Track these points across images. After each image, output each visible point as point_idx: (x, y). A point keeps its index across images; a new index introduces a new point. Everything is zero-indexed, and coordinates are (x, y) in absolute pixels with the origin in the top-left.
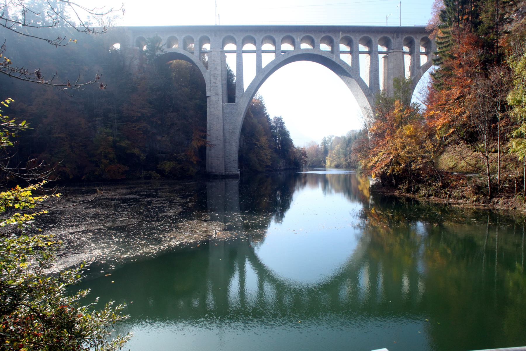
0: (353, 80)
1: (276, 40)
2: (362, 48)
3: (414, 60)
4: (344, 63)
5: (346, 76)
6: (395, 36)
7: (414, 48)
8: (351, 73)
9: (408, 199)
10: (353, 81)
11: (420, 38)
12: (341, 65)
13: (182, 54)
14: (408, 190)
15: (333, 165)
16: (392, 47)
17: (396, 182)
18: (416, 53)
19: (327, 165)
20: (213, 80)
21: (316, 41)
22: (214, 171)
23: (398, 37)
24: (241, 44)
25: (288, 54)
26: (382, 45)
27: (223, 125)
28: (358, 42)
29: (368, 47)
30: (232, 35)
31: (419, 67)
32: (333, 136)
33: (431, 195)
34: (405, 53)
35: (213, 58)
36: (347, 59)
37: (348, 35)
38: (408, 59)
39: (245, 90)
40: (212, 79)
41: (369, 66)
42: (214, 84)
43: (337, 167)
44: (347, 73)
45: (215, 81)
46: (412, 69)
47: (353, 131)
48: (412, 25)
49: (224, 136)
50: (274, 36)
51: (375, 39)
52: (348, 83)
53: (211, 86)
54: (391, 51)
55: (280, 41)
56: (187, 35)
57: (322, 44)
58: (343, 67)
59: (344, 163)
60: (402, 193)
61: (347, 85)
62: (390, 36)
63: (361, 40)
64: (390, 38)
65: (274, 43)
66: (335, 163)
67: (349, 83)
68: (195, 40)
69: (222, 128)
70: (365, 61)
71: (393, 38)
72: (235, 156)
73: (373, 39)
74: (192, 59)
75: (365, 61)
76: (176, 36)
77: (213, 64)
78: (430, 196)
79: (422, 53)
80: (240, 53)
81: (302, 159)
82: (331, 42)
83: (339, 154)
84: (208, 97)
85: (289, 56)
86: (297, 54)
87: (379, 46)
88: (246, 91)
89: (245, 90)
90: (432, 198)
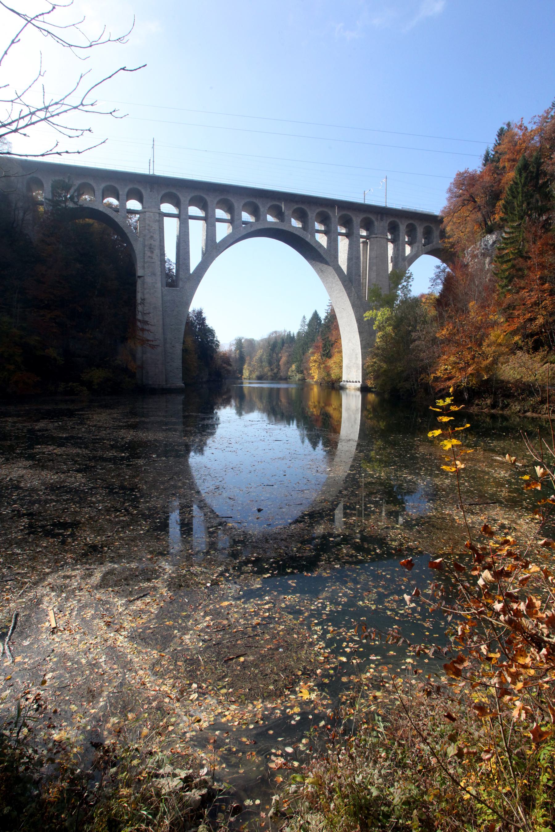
0: (331, 268)
1: (182, 199)
2: (220, 213)
3: (398, 250)
4: (321, 246)
5: (321, 262)
6: (379, 218)
7: (399, 235)
8: (328, 259)
9: (493, 417)
10: (330, 270)
11: (406, 224)
12: (316, 247)
13: (100, 211)
14: (494, 406)
15: (254, 376)
16: (376, 232)
17: (470, 397)
18: (400, 242)
19: (244, 376)
20: (148, 254)
21: (262, 209)
22: (150, 383)
23: (382, 220)
24: (101, 198)
25: (251, 226)
26: (296, 219)
27: (163, 319)
28: (215, 205)
29: (302, 222)
30: (174, 191)
31: (404, 258)
32: (243, 338)
33: (528, 411)
34: (388, 240)
35: (147, 222)
36: (322, 240)
37: (349, 213)
38: (390, 246)
39: (191, 272)
40: (146, 252)
41: (347, 252)
42: (149, 260)
43: (260, 378)
44: (324, 259)
45: (150, 255)
46: (395, 259)
47: (276, 332)
48: (399, 207)
49: (164, 333)
50: (209, 199)
51: (237, 204)
52: (320, 272)
53: (144, 262)
54: (374, 236)
55: (160, 198)
56: (108, 184)
57: (291, 218)
58: (319, 250)
59: (269, 374)
60: (482, 409)
61: (318, 274)
62: (372, 217)
63: (218, 203)
64: (374, 219)
65: (177, 204)
66: (257, 373)
67: (322, 271)
68: (45, 186)
69: (161, 323)
70: (343, 244)
71: (377, 219)
72: (178, 363)
73: (354, 219)
74: (116, 220)
75: (343, 244)
76: (92, 182)
77: (149, 230)
78: (525, 412)
79: (319, 231)
80: (184, 219)
81: (224, 368)
82: (302, 216)
83: (262, 362)
84: (139, 277)
85: (252, 229)
86: (280, 228)
87: (293, 220)
88: (194, 272)
89: (191, 272)
90: (529, 414)
